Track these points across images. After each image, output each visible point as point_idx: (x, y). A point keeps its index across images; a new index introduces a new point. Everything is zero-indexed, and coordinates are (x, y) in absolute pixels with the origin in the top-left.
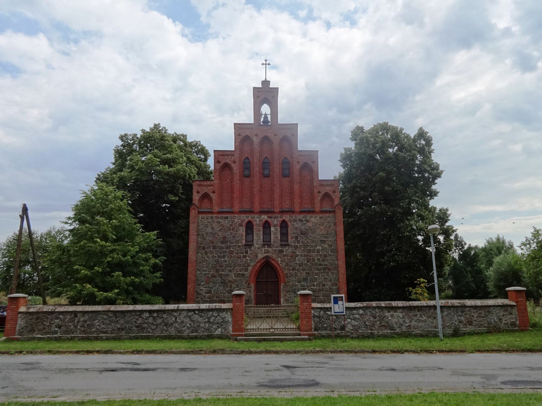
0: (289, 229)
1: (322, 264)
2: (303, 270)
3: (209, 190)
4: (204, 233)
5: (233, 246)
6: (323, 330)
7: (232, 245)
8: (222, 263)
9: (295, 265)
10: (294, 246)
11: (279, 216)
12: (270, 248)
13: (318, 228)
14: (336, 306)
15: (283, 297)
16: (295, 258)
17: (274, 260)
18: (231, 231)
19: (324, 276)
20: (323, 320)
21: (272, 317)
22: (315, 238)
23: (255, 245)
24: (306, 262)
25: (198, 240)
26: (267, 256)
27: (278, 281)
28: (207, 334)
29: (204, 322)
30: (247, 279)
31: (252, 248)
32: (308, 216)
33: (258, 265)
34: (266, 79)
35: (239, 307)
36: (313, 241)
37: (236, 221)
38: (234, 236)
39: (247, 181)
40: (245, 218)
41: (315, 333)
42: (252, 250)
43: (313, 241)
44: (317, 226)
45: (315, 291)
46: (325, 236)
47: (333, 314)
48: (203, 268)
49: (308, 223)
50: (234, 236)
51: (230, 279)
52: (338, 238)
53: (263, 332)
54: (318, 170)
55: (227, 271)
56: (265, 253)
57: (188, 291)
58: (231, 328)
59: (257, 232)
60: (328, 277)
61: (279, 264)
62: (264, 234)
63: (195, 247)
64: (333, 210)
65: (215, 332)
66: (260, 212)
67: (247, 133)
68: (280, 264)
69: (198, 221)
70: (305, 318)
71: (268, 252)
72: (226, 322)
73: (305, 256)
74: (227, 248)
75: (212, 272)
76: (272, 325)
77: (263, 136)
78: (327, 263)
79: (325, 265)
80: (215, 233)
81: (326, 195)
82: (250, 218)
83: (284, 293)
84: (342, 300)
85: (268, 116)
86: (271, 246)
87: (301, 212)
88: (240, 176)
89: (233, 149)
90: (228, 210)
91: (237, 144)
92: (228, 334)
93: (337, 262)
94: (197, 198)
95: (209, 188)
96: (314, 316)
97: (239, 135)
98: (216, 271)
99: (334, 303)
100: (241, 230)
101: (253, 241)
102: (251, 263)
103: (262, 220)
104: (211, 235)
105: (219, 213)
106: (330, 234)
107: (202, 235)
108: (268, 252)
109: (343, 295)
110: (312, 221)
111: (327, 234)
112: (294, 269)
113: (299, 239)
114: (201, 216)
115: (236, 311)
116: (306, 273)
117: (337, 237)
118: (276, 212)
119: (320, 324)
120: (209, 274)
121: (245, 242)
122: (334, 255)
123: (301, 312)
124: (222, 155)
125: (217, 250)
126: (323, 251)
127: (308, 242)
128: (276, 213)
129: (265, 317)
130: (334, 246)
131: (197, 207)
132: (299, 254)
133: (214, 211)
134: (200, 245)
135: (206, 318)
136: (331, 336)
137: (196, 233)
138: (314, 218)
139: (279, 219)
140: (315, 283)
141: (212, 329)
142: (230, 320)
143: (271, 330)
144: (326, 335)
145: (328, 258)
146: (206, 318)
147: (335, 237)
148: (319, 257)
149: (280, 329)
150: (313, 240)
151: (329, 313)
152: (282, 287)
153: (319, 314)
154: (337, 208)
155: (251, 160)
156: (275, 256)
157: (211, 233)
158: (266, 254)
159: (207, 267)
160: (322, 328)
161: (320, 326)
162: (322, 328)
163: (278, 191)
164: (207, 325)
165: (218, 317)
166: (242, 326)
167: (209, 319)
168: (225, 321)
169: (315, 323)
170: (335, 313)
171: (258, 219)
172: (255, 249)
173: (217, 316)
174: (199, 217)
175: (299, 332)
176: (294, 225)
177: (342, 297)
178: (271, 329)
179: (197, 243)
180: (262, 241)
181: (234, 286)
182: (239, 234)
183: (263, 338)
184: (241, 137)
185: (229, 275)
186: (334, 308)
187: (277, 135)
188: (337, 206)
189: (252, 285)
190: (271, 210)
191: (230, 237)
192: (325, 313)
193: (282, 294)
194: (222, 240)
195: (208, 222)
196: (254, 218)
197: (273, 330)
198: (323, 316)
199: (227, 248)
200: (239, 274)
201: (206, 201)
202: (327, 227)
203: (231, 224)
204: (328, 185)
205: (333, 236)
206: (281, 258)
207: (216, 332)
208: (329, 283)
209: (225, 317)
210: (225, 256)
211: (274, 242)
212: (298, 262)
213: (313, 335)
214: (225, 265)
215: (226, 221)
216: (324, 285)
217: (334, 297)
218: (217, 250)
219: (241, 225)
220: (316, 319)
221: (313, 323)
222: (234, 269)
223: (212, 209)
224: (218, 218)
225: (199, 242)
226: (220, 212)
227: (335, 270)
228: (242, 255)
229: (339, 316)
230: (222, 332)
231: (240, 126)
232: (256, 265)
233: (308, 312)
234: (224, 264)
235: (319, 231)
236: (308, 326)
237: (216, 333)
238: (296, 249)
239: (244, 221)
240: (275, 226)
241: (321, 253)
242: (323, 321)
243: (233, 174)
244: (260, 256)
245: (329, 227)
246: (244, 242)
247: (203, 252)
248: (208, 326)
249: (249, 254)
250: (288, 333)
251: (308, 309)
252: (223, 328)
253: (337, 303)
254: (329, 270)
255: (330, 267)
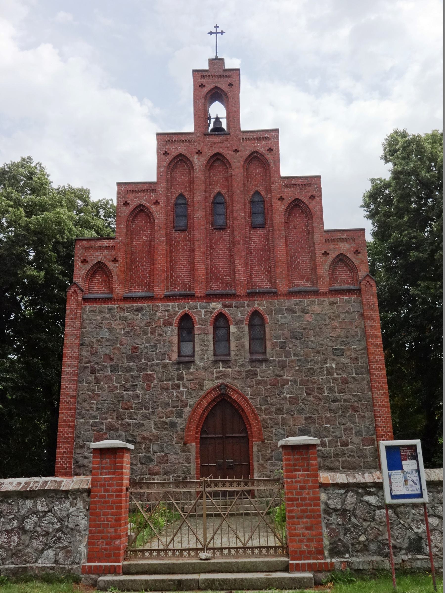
0: (267, 329)
1: (339, 398)
2: (300, 412)
3: (105, 256)
4: (94, 340)
5: (152, 365)
6: (358, 551)
7: (150, 363)
8: (129, 401)
9: (282, 402)
10: (279, 362)
11: (246, 302)
12: (229, 367)
13: (328, 324)
14: (397, 475)
15: (259, 471)
16: (282, 386)
17: (237, 392)
18: (149, 335)
19: (344, 424)
20: (353, 520)
21: (205, 516)
22: (321, 344)
23: (198, 362)
24: (305, 394)
25: (80, 355)
26: (222, 384)
27: (246, 437)
28: (12, 566)
29: (6, 530)
30: (182, 433)
31: (192, 370)
32: (306, 302)
33: (205, 403)
34: (216, 56)
35: (111, 485)
36: (318, 352)
37: (159, 314)
38: (155, 346)
39: (181, 237)
40: (177, 309)
41: (334, 560)
42: (191, 374)
43: (318, 352)
44: (325, 320)
45: (327, 457)
46: (343, 341)
47: (388, 500)
48: (90, 412)
49: (307, 315)
50: (155, 346)
51: (145, 434)
52: (370, 344)
53: (180, 561)
54: (321, 211)
55: (139, 416)
56: (217, 378)
57: (58, 460)
58: (83, 549)
59: (202, 336)
60: (352, 426)
61: (247, 401)
62: (216, 340)
63: (75, 368)
64: (357, 287)
65: (36, 562)
66: (207, 295)
67: (182, 149)
68: (250, 400)
69: (81, 318)
70: (301, 517)
71: (225, 376)
72: (72, 529)
73: (302, 382)
74: (141, 369)
75: (109, 420)
76: (205, 538)
77: (211, 153)
78: (350, 397)
79: (345, 401)
80: (117, 340)
81: (341, 260)
82: (187, 309)
83: (261, 461)
84: (415, 457)
85: (221, 120)
86: (230, 364)
87: (291, 294)
88: (167, 228)
89: (154, 179)
90: (144, 294)
91: (162, 170)
92: (75, 566)
93: (370, 393)
94: (83, 272)
95: (107, 253)
96: (329, 511)
97: (166, 154)
98: (117, 418)
99: (391, 467)
100: (169, 334)
101: (193, 356)
102: (189, 400)
103: (211, 313)
104: (108, 344)
105: (126, 299)
106: (353, 336)
107: (90, 344)
108: (225, 376)
109: (417, 442)
110: (313, 311)
111: (347, 337)
112: (279, 411)
113: (287, 349)
114: (88, 307)
115: (101, 497)
116: (306, 419)
117: (367, 342)
118: (239, 294)
119: (345, 534)
120: (103, 423)
121: (176, 357)
122: (363, 379)
123: (289, 499)
124: (133, 191)
125: (120, 373)
126: (339, 372)
127: (307, 355)
128: (241, 297)
129: (224, 514)
130: (363, 360)
131: (80, 289)
132: (289, 378)
133: (115, 297)
134: (86, 365)
135: (13, 519)
136: (383, 570)
137: (77, 341)
138: (319, 305)
139: (247, 308)
140: (327, 439)
141: (29, 550)
142: (83, 523)
143: (203, 555)
144: (366, 567)
145: (350, 386)
146: (13, 519)
147: (363, 343)
148: (332, 385)
149: (229, 549)
150: (318, 349)
151: (372, 499)
152: (255, 449)
153: (343, 504)
154: (363, 283)
155: (189, 199)
156: (238, 384)
157: (108, 340)
158: (221, 381)
159: (98, 409)
160: (353, 545)
161: (347, 539)
162: (353, 545)
163: (243, 253)
164: (16, 538)
165: (49, 517)
166: (117, 542)
167: (23, 520)
168: (67, 527)
169: (332, 530)
170: (394, 497)
171: (203, 311)
172: (197, 370)
173: (46, 513)
174: (84, 309)
175: (286, 559)
176: (278, 321)
177: (413, 447)
178: (202, 549)
179: (80, 361)
180: (212, 354)
181: (155, 449)
182: (164, 340)
183: (173, 580)
184: (169, 159)
185: (143, 425)
186: (390, 480)
187: (238, 151)
188: (363, 280)
189: (193, 446)
190: (229, 292)
191: (146, 347)
192: (361, 501)
193: (255, 464)
194: (130, 353)
195: (103, 319)
196: (195, 308)
197: (208, 554)
198: (354, 509)
199: (141, 369)
200: (165, 423)
201: (100, 278)
202: (345, 322)
203: (149, 320)
204: (343, 240)
205: (359, 341)
206: (252, 387)
207: (40, 561)
208: (356, 440)
209: (68, 516)
210: (136, 385)
211: (237, 355)
212: (288, 396)
213: (330, 568)
214: (136, 404)
215: (138, 315)
216: (345, 444)
217: (388, 448)
218: (120, 373)
219: (168, 323)
220: (333, 518)
221: (325, 531)
222: (153, 412)
223: (112, 293)
224: (123, 310)
225: (84, 358)
226: (127, 298)
227: (368, 411)
228: (170, 382)
229: (402, 509)
230: (56, 562)
231: (168, 138)
232: (199, 404)
233: (311, 499)
234: (134, 403)
235: (329, 330)
236: (309, 540)
237: (40, 563)
238: (283, 369)
239: (175, 314)
240: (238, 323)
241: (335, 375)
242: (355, 526)
243: (152, 225)
244: (208, 385)
245: (351, 322)
246: (175, 356)
247: (91, 378)
248: (19, 544)
249: (185, 380)
250: (250, 562)
251: (310, 488)
252: (62, 548)
253: (400, 468)
254: (355, 410)
255: (356, 404)
